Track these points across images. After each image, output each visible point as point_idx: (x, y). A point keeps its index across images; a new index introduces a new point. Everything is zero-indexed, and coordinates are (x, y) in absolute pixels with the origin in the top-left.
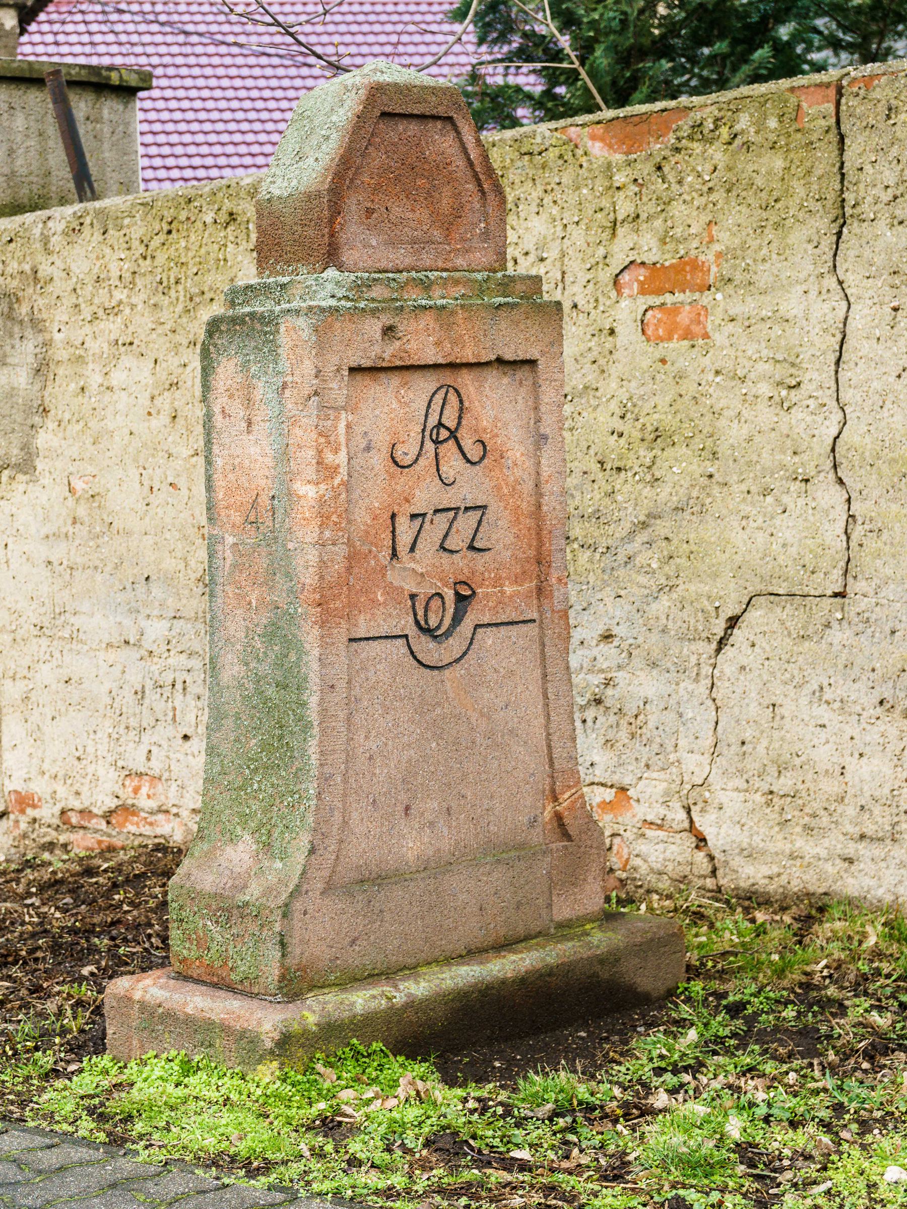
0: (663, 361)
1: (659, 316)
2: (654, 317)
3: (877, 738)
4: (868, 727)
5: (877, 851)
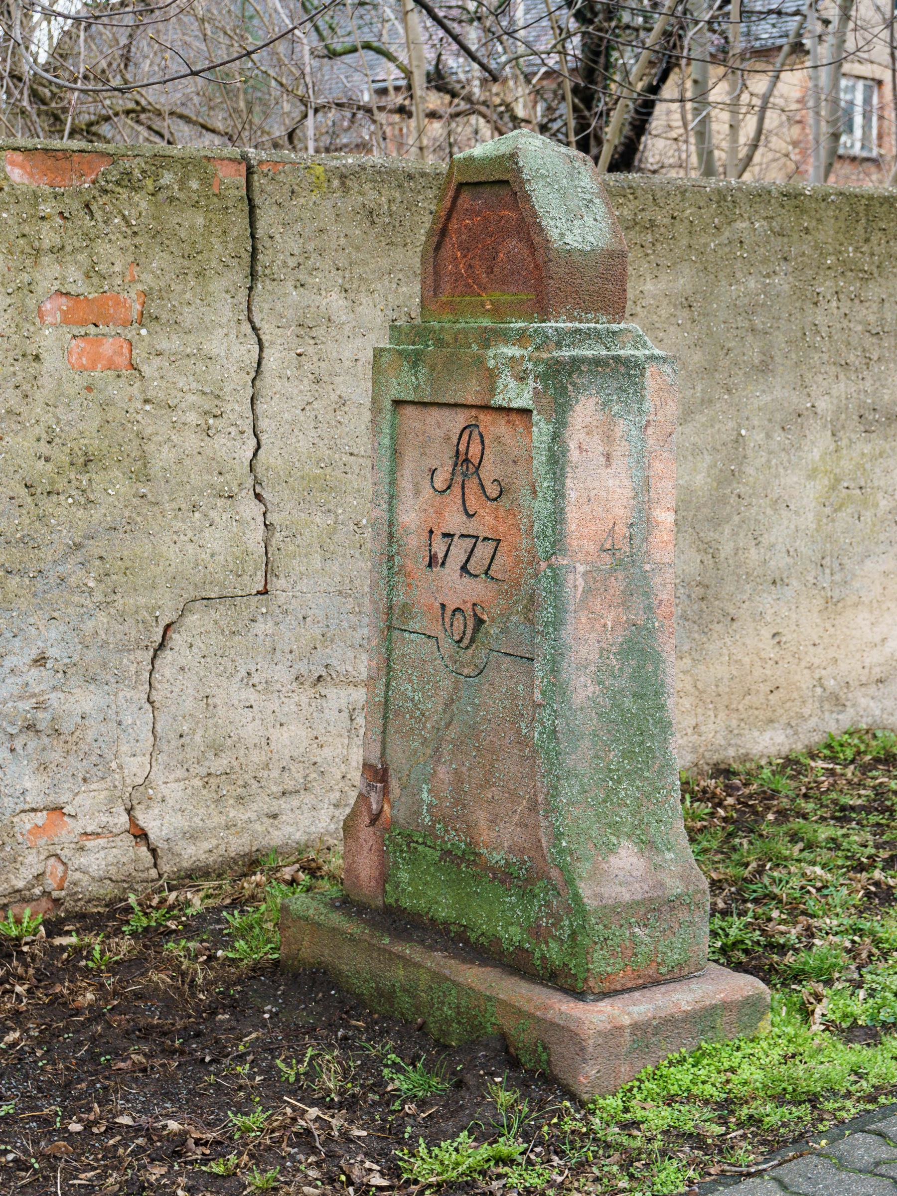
0: (89, 389)
1: (82, 345)
2: (78, 347)
3: (294, 708)
4: (286, 700)
5: (295, 802)
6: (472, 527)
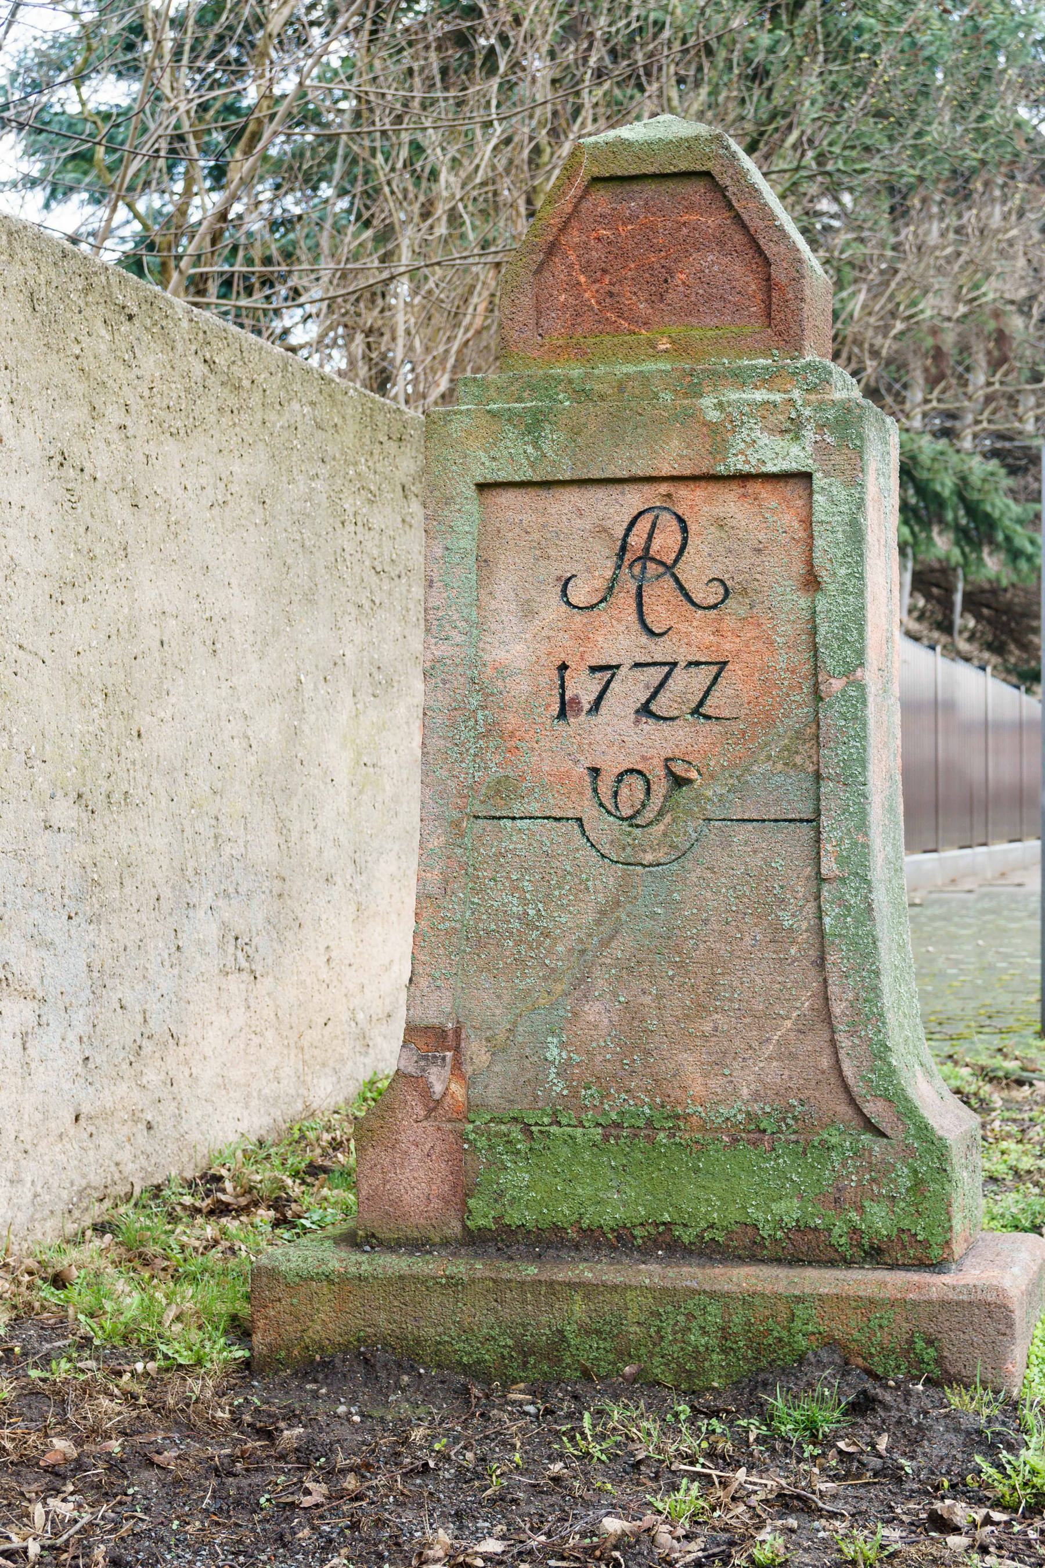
6: (660, 651)
